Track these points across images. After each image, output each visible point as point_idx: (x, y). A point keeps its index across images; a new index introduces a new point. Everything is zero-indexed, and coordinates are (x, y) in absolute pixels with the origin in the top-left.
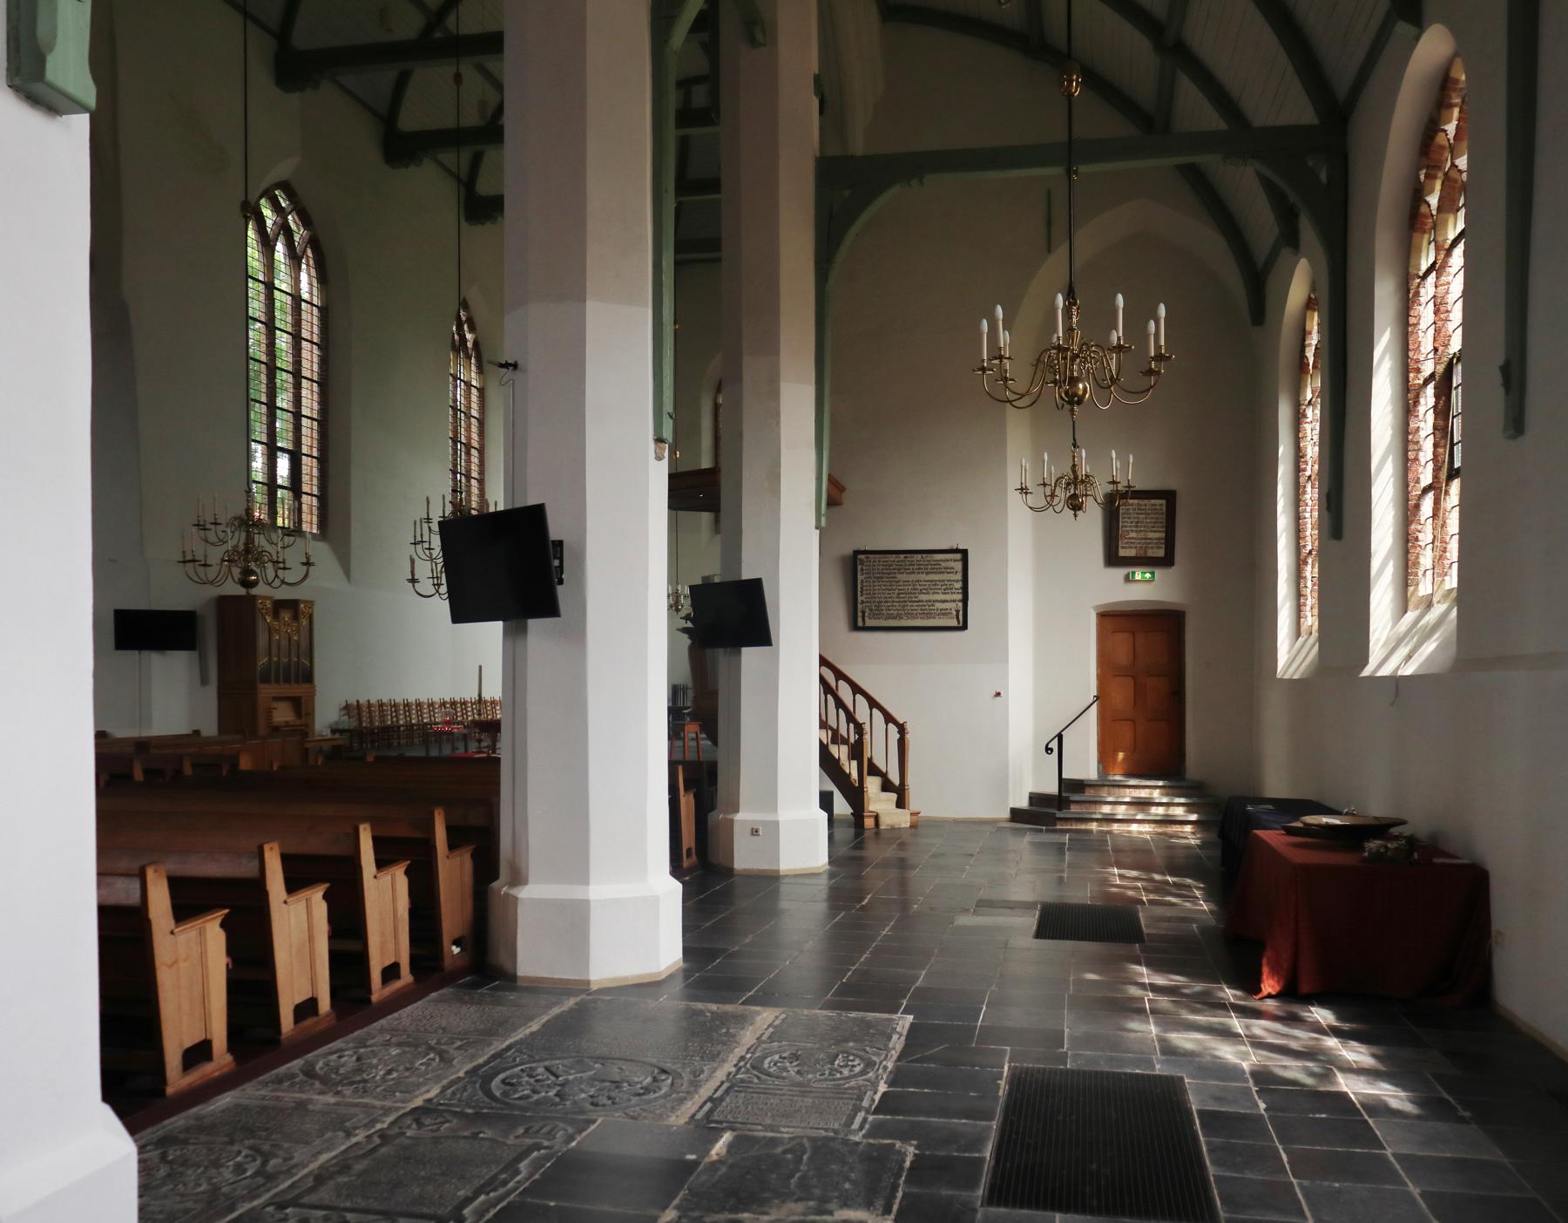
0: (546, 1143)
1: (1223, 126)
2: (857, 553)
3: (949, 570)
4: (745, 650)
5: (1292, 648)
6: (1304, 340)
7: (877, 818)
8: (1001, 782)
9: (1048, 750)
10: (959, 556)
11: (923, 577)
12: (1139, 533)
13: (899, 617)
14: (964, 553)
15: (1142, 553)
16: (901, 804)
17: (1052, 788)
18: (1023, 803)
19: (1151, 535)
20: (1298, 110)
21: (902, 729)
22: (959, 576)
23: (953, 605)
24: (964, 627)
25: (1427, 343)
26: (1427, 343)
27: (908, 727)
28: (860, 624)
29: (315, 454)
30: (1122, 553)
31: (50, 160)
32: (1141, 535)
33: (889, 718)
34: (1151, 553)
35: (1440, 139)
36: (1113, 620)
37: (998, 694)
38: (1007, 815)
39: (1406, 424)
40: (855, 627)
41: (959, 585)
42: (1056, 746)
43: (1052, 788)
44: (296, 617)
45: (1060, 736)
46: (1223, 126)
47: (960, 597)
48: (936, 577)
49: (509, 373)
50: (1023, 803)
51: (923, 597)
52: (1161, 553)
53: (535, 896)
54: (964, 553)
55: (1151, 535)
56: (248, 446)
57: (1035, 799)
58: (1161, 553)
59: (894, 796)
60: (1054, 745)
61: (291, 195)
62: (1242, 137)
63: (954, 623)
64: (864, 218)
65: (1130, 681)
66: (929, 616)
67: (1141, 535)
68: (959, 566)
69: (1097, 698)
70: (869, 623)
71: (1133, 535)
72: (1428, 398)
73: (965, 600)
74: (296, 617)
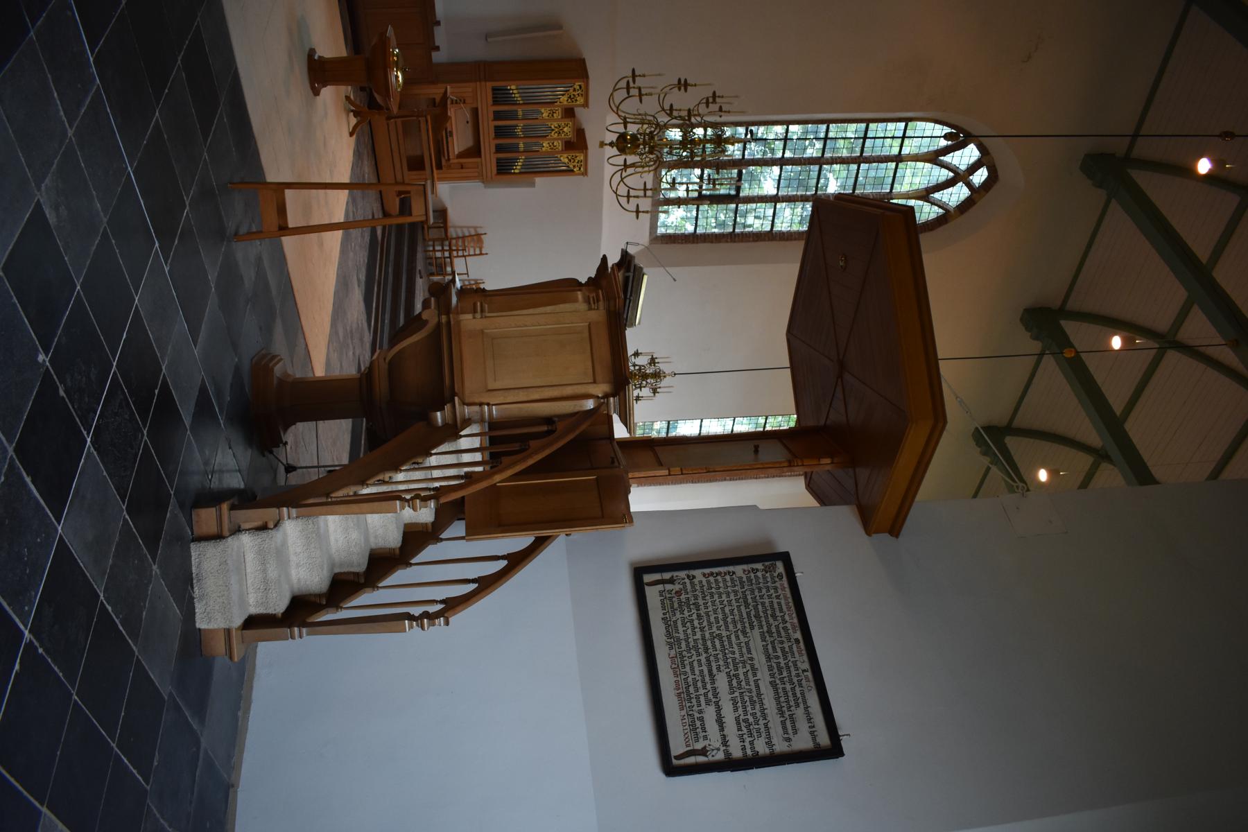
3: (790, 726)
4: (632, 510)
5: (480, 469)
10: (824, 739)
11: (764, 677)
13: (673, 642)
22: (780, 747)
28: (647, 578)
29: (734, 206)
40: (639, 572)
41: (762, 748)
44: (569, 146)
47: (737, 753)
51: (722, 682)
53: (1139, 181)
54: (834, 750)
56: (899, 120)
61: (987, 185)
63: (677, 746)
64: (549, 309)
66: (684, 696)
68: (802, 742)
70: (652, 594)
74: (569, 146)
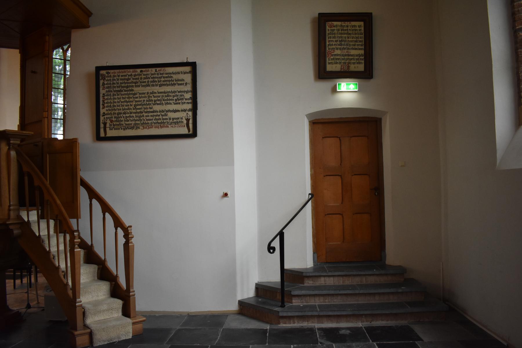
2: (98, 69)
3: (180, 82)
7: (91, 335)
8: (230, 278)
9: (271, 249)
10: (188, 69)
11: (156, 89)
12: (344, 48)
13: (136, 127)
14: (193, 65)
15: (346, 68)
16: (126, 312)
17: (274, 277)
19: (353, 52)
21: (127, 235)
22: (189, 88)
24: (194, 135)
27: (134, 231)
28: (102, 135)
30: (330, 68)
31: (12, 57)
32: (345, 52)
33: (118, 223)
34: (353, 68)
36: (326, 127)
37: (226, 195)
38: (234, 307)
41: (189, 95)
42: (277, 244)
43: (274, 277)
45: (281, 234)
47: (190, 106)
48: (168, 89)
51: (157, 108)
52: (361, 68)
55: (353, 52)
58: (361, 68)
59: (118, 303)
60: (276, 244)
65: (338, 180)
66: (162, 125)
67: (345, 52)
68: (188, 78)
69: (312, 195)
70: (111, 133)
71: (338, 52)
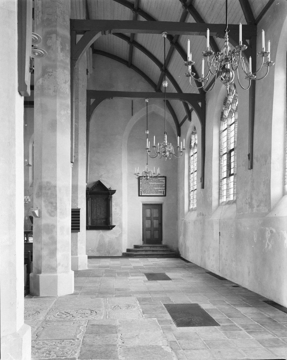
0: (142, 306)
1: (176, 92)
6: (191, 141)
18: (125, 251)
20: (195, 90)
22: (164, 183)
23: (163, 190)
25: (225, 145)
26: (225, 145)
28: (140, 195)
35: (228, 102)
39: (220, 163)
46: (176, 92)
47: (164, 188)
49: (131, 114)
50: (125, 251)
57: (128, 250)
62: (180, 95)
68: (164, 181)
70: (142, 195)
72: (225, 157)
73: (166, 189)
